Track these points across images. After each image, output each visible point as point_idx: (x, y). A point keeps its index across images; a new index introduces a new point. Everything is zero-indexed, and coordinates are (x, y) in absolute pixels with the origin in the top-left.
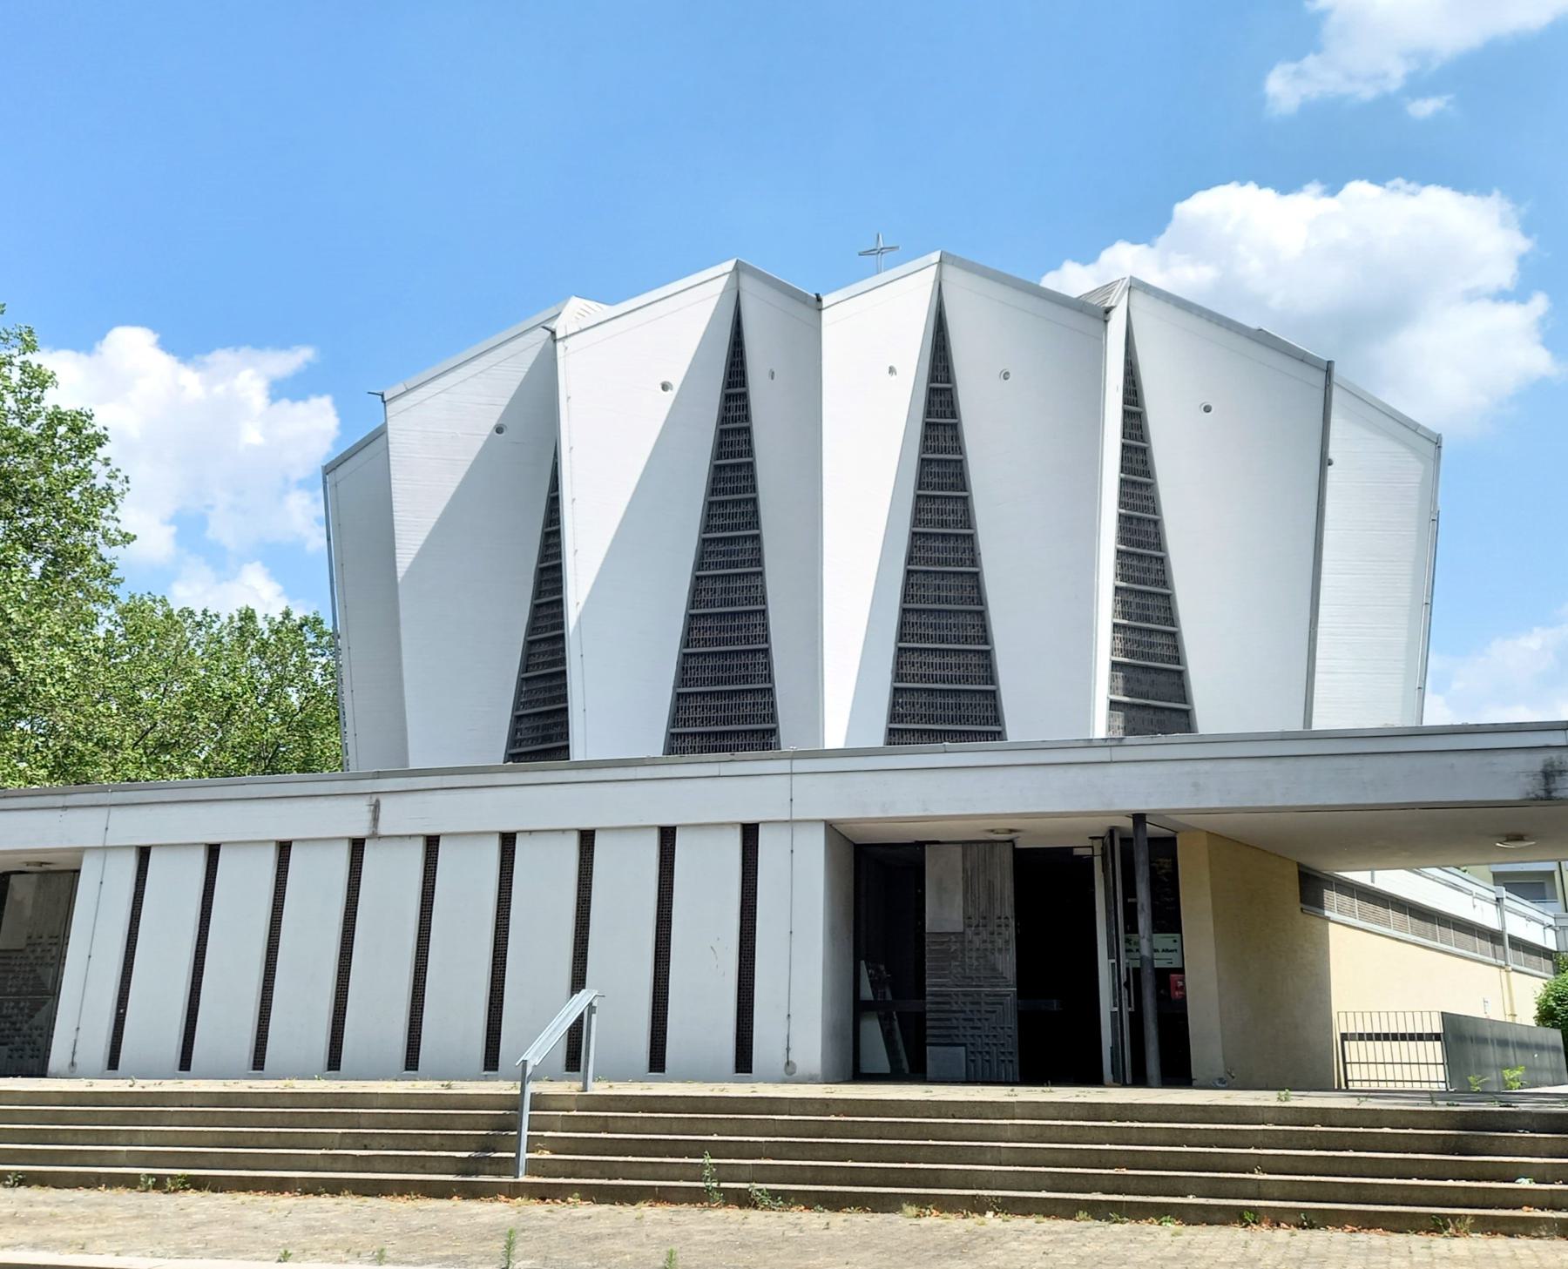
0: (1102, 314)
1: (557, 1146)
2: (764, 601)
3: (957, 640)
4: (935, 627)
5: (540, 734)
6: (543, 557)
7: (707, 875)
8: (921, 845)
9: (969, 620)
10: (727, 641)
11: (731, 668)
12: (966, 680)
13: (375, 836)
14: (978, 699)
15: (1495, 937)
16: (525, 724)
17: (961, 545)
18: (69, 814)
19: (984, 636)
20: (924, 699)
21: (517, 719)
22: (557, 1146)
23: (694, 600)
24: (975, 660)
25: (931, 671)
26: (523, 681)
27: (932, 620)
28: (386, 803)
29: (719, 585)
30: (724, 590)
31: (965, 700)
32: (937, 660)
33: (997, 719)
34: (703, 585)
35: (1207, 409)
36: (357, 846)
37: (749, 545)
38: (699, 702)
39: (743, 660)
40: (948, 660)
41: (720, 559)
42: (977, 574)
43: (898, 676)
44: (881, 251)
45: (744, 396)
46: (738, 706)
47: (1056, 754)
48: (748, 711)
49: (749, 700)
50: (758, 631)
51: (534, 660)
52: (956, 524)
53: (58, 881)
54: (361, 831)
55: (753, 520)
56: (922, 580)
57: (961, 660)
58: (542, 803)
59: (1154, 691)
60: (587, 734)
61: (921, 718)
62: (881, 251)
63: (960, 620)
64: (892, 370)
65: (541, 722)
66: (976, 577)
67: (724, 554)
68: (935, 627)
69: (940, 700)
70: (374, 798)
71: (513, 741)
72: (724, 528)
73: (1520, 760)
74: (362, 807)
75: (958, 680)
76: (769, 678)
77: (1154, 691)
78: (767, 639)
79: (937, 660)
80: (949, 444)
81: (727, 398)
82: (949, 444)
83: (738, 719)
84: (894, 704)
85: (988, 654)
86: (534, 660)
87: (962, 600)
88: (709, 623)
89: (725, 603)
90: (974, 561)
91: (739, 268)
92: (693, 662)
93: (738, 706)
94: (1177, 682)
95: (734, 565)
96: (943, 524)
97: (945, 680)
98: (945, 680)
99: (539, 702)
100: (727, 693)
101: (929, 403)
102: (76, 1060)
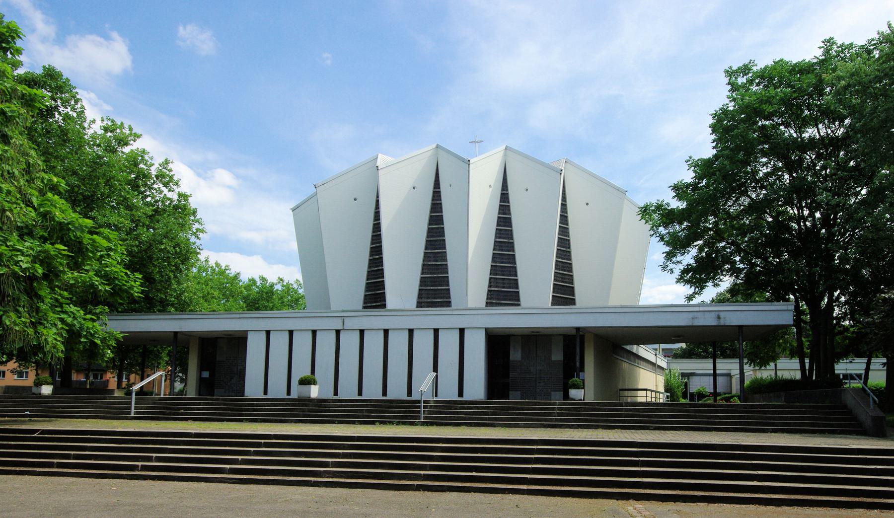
1: (429, 413)
6: (429, 244)
7: (374, 343)
8: (217, 338)
15: (654, 364)
18: (243, 320)
22: (429, 413)
28: (346, 319)
33: (519, 300)
35: (355, 199)
36: (338, 332)
44: (477, 142)
47: (535, 309)
53: (238, 341)
58: (375, 320)
59: (564, 293)
60: (392, 301)
61: (496, 299)
62: (477, 142)
71: (365, 303)
73: (686, 315)
74: (340, 321)
77: (564, 293)
84: (419, 294)
91: (438, 147)
94: (571, 291)
97: (503, 287)
98: (503, 287)
100: (434, 289)
101: (433, 196)
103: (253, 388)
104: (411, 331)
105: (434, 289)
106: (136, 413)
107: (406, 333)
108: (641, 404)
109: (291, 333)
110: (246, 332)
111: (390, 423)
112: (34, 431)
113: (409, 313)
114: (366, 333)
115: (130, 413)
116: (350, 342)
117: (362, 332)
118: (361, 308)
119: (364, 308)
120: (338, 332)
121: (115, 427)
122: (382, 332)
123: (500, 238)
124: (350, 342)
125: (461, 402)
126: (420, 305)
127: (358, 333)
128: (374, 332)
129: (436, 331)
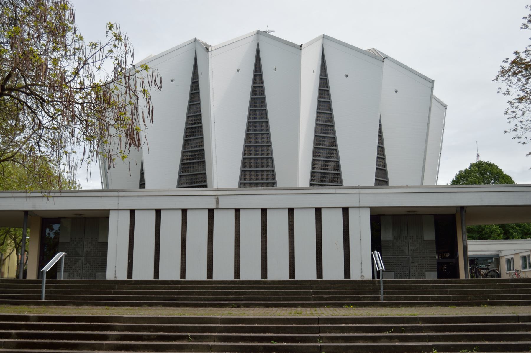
0: (299, 47)
2: (270, 142)
3: (329, 157)
4: (323, 153)
5: (190, 181)
9: (332, 152)
10: (258, 155)
11: (259, 163)
12: (332, 169)
13: (217, 209)
14: (336, 176)
16: (183, 178)
17: (330, 128)
19: (337, 157)
20: (320, 175)
21: (180, 176)
23: (246, 141)
24: (334, 164)
25: (322, 167)
26: (182, 164)
27: (322, 151)
28: (220, 197)
29: (254, 137)
30: (256, 138)
31: (331, 176)
32: (323, 163)
34: (249, 136)
35: (172, 81)
36: (211, 212)
37: (264, 124)
38: (249, 173)
39: (264, 161)
40: (326, 163)
41: (254, 128)
42: (334, 138)
43: (313, 168)
45: (261, 75)
46: (262, 175)
48: (266, 177)
49: (266, 173)
50: (269, 152)
51: (185, 158)
52: (328, 121)
54: (213, 206)
55: (265, 116)
56: (251, 136)
57: (330, 164)
63: (330, 151)
64: (347, 76)
65: (190, 178)
66: (334, 138)
67: (255, 127)
68: (323, 153)
69: (324, 176)
70: (216, 197)
72: (255, 118)
75: (329, 169)
76: (273, 166)
78: (271, 154)
79: (323, 163)
80: (326, 96)
81: (255, 76)
82: (326, 96)
83: (262, 179)
85: (338, 162)
86: (185, 158)
87: (331, 145)
88: (251, 149)
89: (257, 142)
90: (334, 133)
92: (246, 161)
93: (262, 175)
95: (259, 130)
96: (324, 121)
99: (188, 171)
100: (258, 168)
102: (116, 275)
103: (115, 270)
104: (318, 211)
105: (258, 168)
106: (46, 298)
107: (180, 214)
108: (506, 281)
109: (158, 212)
110: (108, 211)
111: (349, 305)
112: (26, 318)
113: (116, 194)
114: (242, 212)
115: (40, 298)
116: (171, 224)
117: (237, 211)
118: (372, 183)
119: (311, 185)
120: (211, 212)
121: (195, 314)
122: (260, 212)
123: (320, 121)
124: (171, 224)
125: (265, 283)
126: (242, 184)
127: (313, 212)
128: (147, 211)
129: (318, 211)
